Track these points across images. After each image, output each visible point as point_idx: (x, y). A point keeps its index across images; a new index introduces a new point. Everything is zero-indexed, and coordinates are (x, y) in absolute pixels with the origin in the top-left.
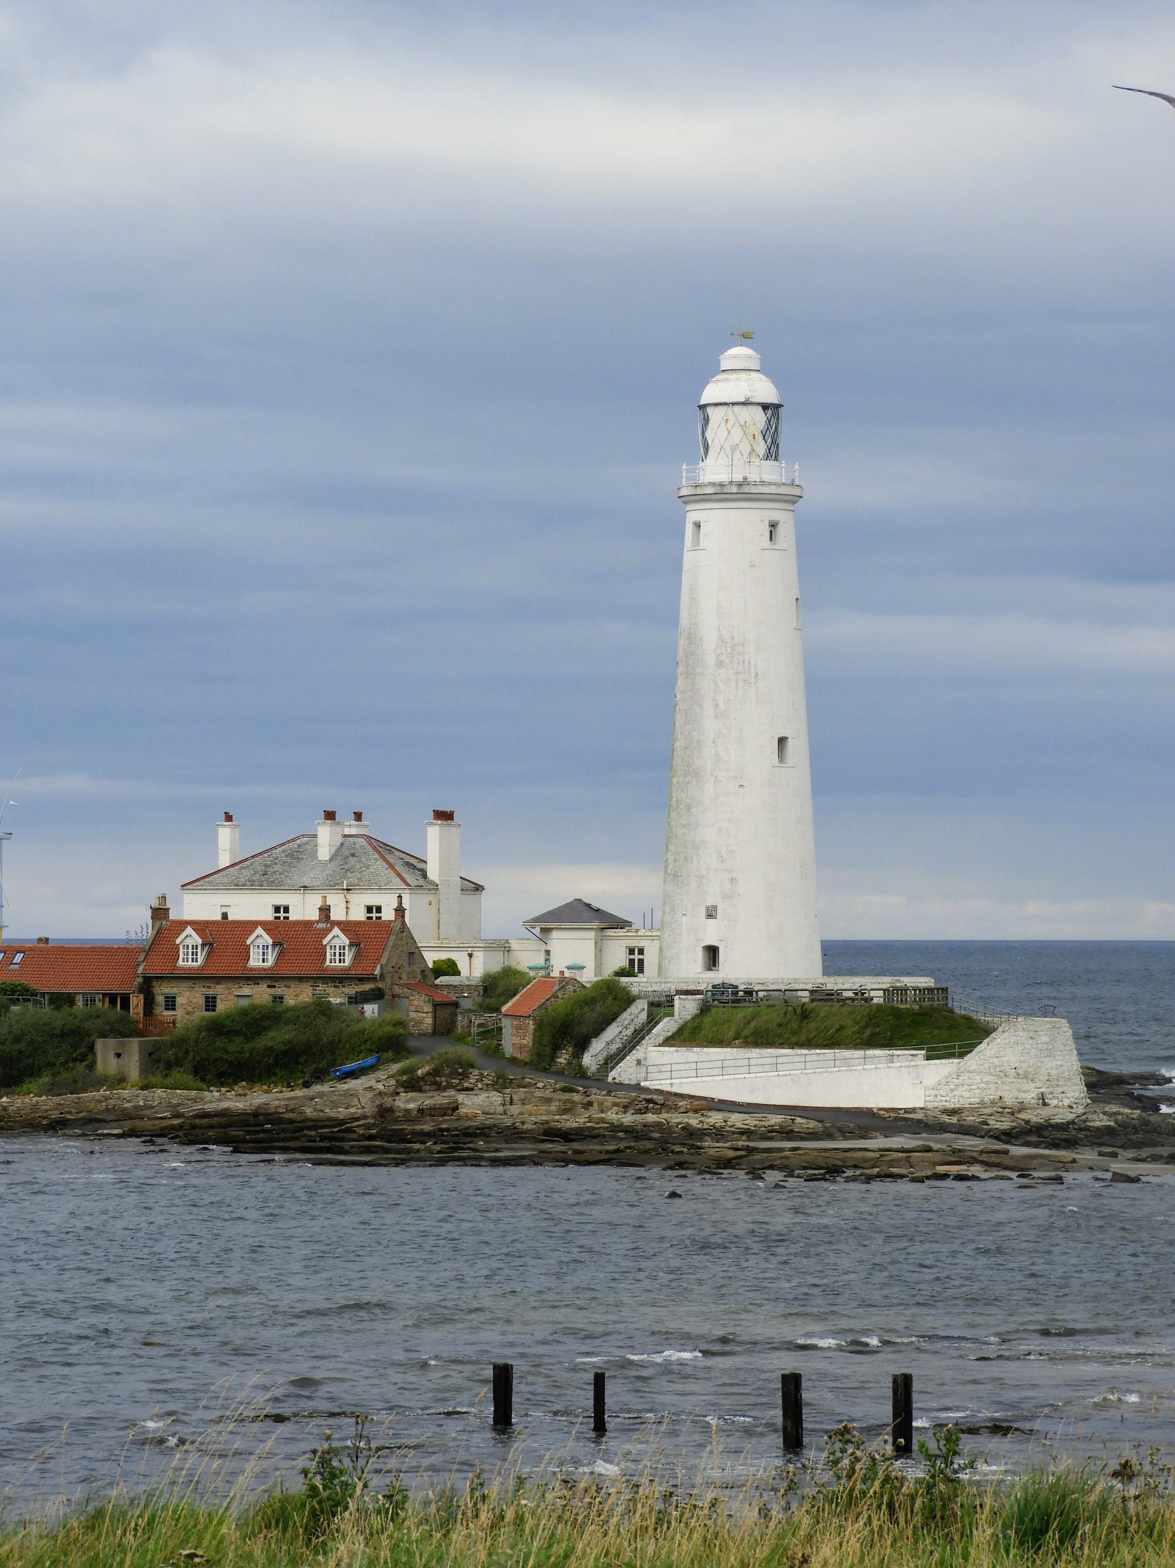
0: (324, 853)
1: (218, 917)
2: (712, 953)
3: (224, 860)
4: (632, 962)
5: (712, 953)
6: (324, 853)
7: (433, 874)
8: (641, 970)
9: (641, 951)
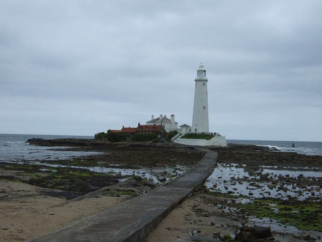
2: (196, 129)
5: (196, 129)
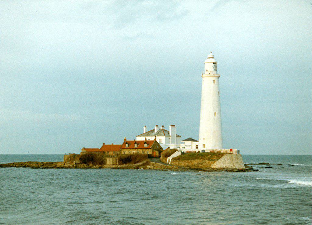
0: (156, 131)
1: (134, 140)
2: (204, 145)
3: (144, 132)
4: (196, 147)
5: (204, 145)
6: (156, 131)
7: (170, 134)
8: (198, 148)
9: (198, 145)
